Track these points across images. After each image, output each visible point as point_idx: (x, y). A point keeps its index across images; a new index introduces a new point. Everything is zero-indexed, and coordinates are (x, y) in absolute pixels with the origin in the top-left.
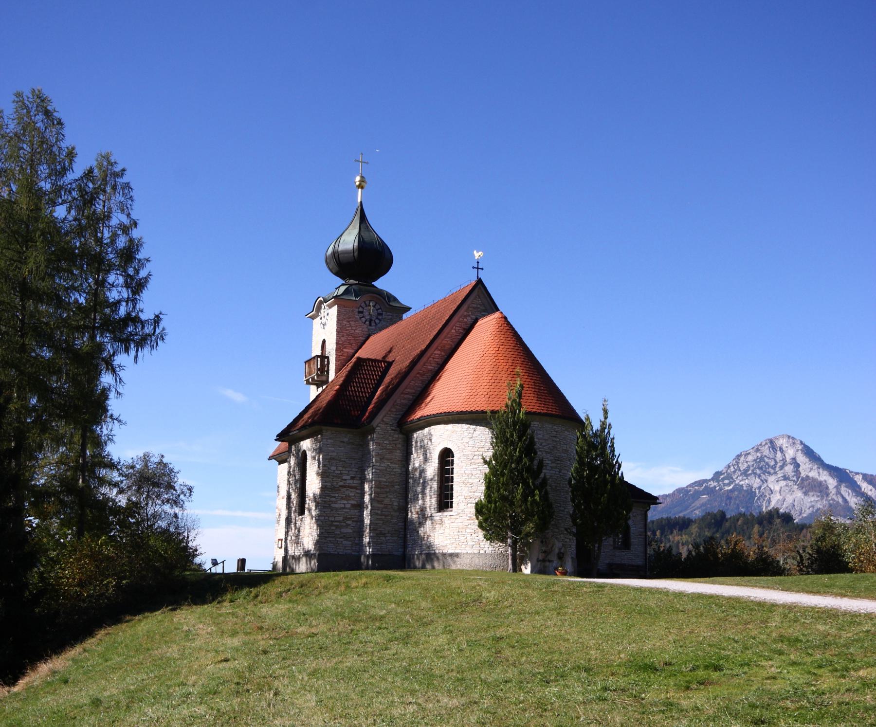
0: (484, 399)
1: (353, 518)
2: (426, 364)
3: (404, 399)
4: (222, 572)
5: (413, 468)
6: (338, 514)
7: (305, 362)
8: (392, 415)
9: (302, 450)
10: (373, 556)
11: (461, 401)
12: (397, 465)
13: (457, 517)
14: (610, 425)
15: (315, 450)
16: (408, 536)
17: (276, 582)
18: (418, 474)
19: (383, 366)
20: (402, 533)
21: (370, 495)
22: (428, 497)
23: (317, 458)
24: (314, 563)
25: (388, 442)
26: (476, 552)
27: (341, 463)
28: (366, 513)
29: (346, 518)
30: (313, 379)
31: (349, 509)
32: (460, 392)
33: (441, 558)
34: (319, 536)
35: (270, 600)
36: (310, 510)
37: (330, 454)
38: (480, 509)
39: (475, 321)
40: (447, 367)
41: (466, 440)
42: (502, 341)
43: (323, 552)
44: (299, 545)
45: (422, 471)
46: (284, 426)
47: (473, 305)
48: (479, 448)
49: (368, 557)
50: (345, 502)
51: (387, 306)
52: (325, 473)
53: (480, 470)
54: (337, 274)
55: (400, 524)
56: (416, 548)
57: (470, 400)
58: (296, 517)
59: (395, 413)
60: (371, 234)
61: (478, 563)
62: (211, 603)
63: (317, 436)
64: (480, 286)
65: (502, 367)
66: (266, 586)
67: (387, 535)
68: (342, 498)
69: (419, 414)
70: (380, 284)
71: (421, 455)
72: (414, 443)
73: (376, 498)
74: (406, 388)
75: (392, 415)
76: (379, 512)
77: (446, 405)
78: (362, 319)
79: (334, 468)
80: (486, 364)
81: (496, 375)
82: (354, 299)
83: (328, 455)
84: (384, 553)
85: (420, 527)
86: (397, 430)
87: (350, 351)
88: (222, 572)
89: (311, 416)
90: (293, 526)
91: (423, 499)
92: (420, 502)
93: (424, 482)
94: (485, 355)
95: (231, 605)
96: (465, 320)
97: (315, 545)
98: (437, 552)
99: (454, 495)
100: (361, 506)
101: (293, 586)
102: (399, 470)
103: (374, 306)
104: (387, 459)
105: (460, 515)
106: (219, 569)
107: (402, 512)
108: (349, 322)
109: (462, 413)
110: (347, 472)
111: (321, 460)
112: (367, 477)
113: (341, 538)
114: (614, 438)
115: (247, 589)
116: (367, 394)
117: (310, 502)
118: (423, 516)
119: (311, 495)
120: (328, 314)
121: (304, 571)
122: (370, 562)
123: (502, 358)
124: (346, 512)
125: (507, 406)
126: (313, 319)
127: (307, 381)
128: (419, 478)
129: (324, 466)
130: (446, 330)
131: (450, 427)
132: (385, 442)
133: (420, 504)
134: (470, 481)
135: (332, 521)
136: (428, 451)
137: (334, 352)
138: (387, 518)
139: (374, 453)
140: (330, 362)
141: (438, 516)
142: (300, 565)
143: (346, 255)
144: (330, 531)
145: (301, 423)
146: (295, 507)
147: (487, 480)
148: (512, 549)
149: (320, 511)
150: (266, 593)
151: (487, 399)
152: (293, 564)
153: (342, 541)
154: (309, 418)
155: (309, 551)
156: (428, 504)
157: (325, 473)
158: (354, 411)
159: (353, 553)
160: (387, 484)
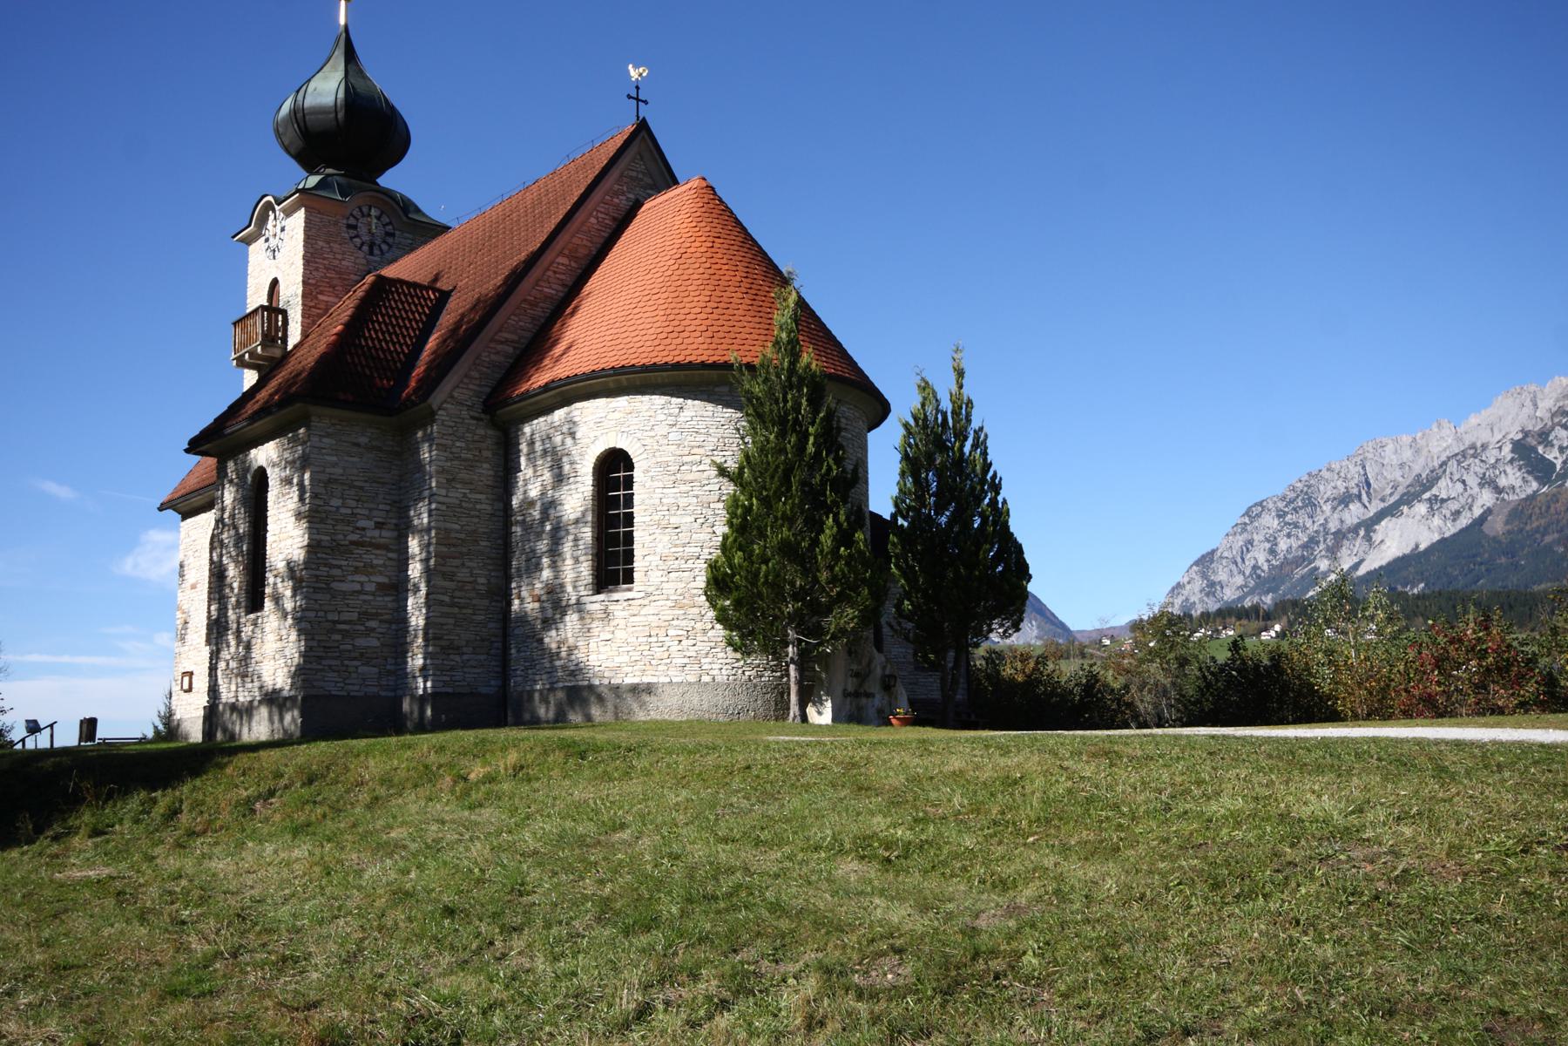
0: (701, 340)
1: (381, 615)
3: (495, 354)
4: (48, 746)
6: (348, 605)
7: (235, 324)
8: (471, 386)
9: (255, 466)
10: (434, 697)
11: (649, 343)
13: (646, 602)
14: (970, 402)
16: (513, 651)
17: (229, 771)
19: (432, 297)
21: (426, 561)
22: (569, 562)
23: (295, 481)
24: (292, 719)
25: (463, 445)
26: (692, 679)
27: (353, 492)
29: (365, 616)
30: (252, 354)
31: (373, 594)
35: (218, 823)
36: (277, 599)
37: (328, 470)
38: (719, 583)
39: (636, 207)
40: (587, 288)
44: (249, 680)
45: (550, 506)
46: (207, 420)
48: (693, 447)
49: (422, 700)
50: (363, 578)
51: (404, 219)
52: (317, 511)
53: (697, 497)
55: (491, 625)
56: (538, 677)
58: (239, 617)
59: (477, 382)
61: (700, 705)
62: (31, 842)
66: (198, 782)
67: (465, 650)
68: (357, 570)
69: (540, 379)
70: (390, 180)
72: (524, 447)
73: (439, 568)
74: (500, 331)
75: (471, 386)
76: (446, 599)
77: (611, 354)
83: (323, 472)
86: (481, 420)
88: (48, 746)
90: (231, 638)
91: (554, 566)
92: (546, 574)
95: (96, 846)
96: (616, 200)
97: (293, 678)
100: (399, 588)
101: (283, 782)
103: (378, 218)
104: (464, 482)
105: (652, 598)
106: (42, 741)
108: (329, 243)
110: (367, 512)
111: (307, 482)
112: (416, 522)
113: (355, 659)
114: (981, 429)
115: (143, 794)
116: (405, 348)
117: (279, 580)
118: (555, 605)
119: (281, 566)
120: (283, 229)
121: (263, 738)
122: (429, 712)
124: (365, 601)
126: (249, 244)
128: (542, 522)
129: (314, 496)
130: (580, 216)
131: (622, 402)
132: (458, 444)
134: (674, 520)
136: (565, 459)
137: (299, 299)
138: (464, 611)
139: (433, 468)
140: (290, 321)
141: (595, 603)
142: (254, 724)
143: (320, 116)
145: (251, 408)
146: (238, 595)
149: (305, 598)
150: (203, 803)
151: (709, 341)
153: (357, 667)
155: (276, 692)
156: (568, 573)
157: (317, 511)
158: (381, 379)
159: (383, 694)
160: (463, 536)
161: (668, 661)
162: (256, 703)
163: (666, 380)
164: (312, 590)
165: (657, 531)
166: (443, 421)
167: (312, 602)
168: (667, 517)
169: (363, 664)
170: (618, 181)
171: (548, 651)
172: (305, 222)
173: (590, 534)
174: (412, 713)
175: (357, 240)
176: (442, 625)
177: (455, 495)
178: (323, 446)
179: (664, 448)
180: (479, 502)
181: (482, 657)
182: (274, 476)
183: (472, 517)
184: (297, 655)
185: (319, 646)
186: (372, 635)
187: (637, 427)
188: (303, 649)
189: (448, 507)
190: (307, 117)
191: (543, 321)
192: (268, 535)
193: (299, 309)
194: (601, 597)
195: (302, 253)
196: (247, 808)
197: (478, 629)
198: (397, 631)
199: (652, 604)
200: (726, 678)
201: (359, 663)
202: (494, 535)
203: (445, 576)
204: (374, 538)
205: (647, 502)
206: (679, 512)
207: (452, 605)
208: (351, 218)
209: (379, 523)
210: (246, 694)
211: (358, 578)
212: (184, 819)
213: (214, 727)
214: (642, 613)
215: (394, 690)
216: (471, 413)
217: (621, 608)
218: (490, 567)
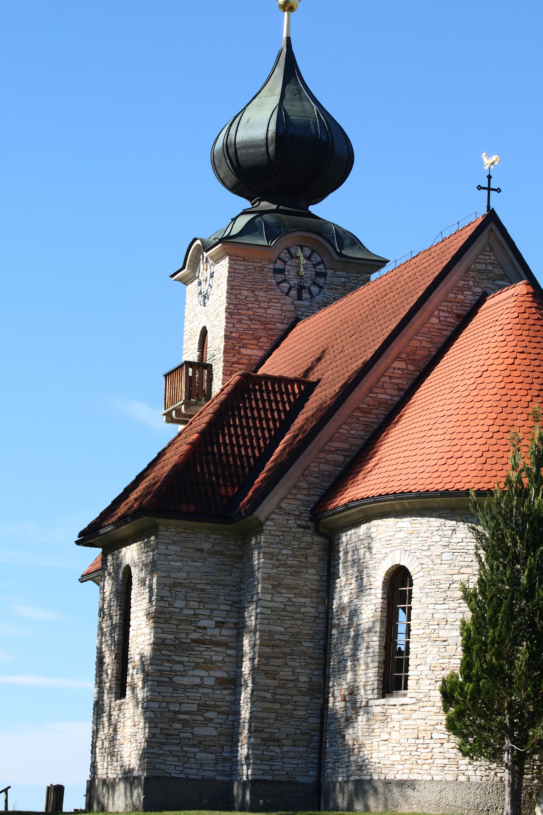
0: (473, 466)
2: (374, 390)
3: (324, 463)
5: (340, 605)
7: (166, 376)
8: (299, 496)
12: (307, 600)
13: (416, 707)
15: (145, 565)
16: (328, 745)
18: (346, 619)
19: (297, 391)
20: (316, 738)
21: (252, 659)
23: (147, 583)
24: (138, 793)
25: (290, 552)
26: (450, 778)
28: (245, 695)
29: (204, 707)
31: (212, 687)
32: (428, 451)
33: (380, 790)
34: (148, 741)
36: (133, 689)
41: (437, 550)
42: (524, 344)
43: (155, 773)
44: (115, 759)
45: (355, 613)
47: (479, 267)
49: (244, 785)
50: (203, 673)
51: (336, 257)
54: (236, 189)
56: (340, 770)
57: (444, 468)
58: (111, 702)
59: (306, 492)
60: (306, 104)
63: (150, 537)
64: (492, 225)
65: (517, 398)
67: (284, 742)
68: (197, 666)
71: (353, 581)
72: (341, 554)
74: (330, 440)
76: (269, 695)
78: (282, 285)
79: (182, 604)
80: (485, 391)
81: (504, 416)
82: (265, 243)
83: (169, 576)
84: (276, 779)
85: (347, 727)
86: (309, 528)
87: (255, 352)
89: (141, 496)
90: (105, 719)
91: (354, 669)
92: (349, 676)
93: (357, 635)
94: (485, 374)
98: (375, 777)
99: (410, 662)
102: (312, 610)
103: (308, 258)
104: (289, 587)
105: (421, 704)
107: (317, 695)
109: (427, 494)
110: (208, 612)
111: (154, 586)
112: (249, 623)
113: (194, 746)
116: (256, 451)
117: (135, 671)
119: (137, 658)
122: (248, 797)
123: (520, 379)
124: (204, 694)
125: (509, 482)
126: (186, 283)
127: (168, 415)
129: (160, 599)
131: (406, 522)
132: (284, 552)
133: (348, 680)
134: (443, 634)
135: (175, 712)
136: (365, 572)
138: (285, 707)
142: (116, 798)
144: (169, 732)
145: (122, 509)
147: (465, 634)
148: (512, 773)
151: (480, 467)
152: (104, 797)
153: (195, 753)
154: (136, 500)
155: (131, 771)
156: (361, 679)
157: (162, 613)
158: (226, 486)
159: (219, 778)
160: (286, 637)
161: (431, 761)
162: (117, 780)
163: (441, 505)
164: (156, 683)
165: (428, 643)
166: (271, 531)
167: (156, 694)
168: (437, 631)
169: (201, 751)
170: (465, 277)
171: (347, 748)
172: (229, 272)
173: (377, 643)
174: (238, 796)
176: (263, 718)
177: (280, 599)
178: (168, 552)
179: (437, 567)
181: (302, 749)
183: (297, 619)
184: (143, 740)
185: (161, 733)
186: (210, 724)
187: (416, 547)
188: (147, 735)
189: (272, 611)
190: (239, 152)
191: (376, 427)
192: (131, 629)
193: (221, 364)
194: (382, 701)
195: (225, 305)
197: (299, 723)
198: (233, 721)
199: (421, 709)
200: (479, 778)
201: (197, 750)
202: (317, 636)
203: (267, 674)
204: (215, 636)
205: (421, 616)
206: (447, 627)
207: (273, 701)
208: (279, 262)
209: (219, 622)
210: (113, 771)
211: (198, 672)
213: (92, 799)
214: (413, 717)
215: (230, 776)
216: (298, 522)
217: (396, 711)
218: (313, 667)
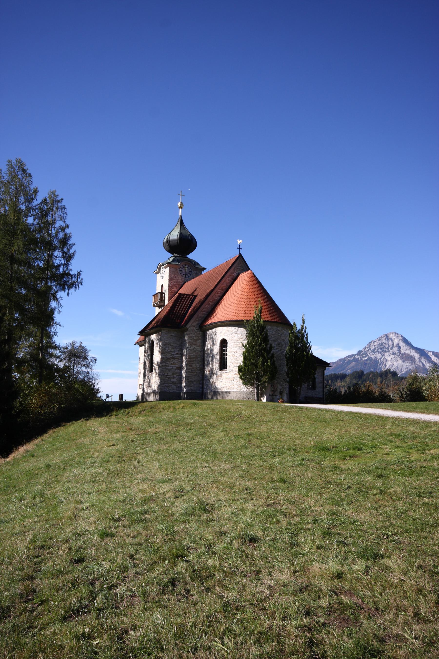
10: (187, 393)
21: (186, 362)
24: (158, 396)
26: (239, 391)
28: (184, 371)
29: (173, 374)
30: (157, 304)
34: (160, 383)
36: (155, 370)
38: (240, 369)
45: (212, 350)
49: (184, 393)
50: (173, 366)
64: (240, 257)
68: (172, 364)
69: (210, 322)
70: (191, 256)
85: (210, 378)
90: (147, 378)
91: (212, 364)
92: (211, 366)
93: (213, 356)
100: (181, 368)
103: (187, 268)
104: (194, 344)
106: (109, 400)
109: (231, 321)
118: (212, 373)
119: (156, 362)
125: (254, 318)
129: (162, 348)
130: (224, 280)
131: (225, 328)
134: (236, 355)
141: (219, 373)
145: (151, 326)
154: (155, 324)
155: (155, 390)
156: (214, 367)
170: (234, 270)
175: (182, 274)
180: (198, 349)
182: (155, 342)
194: (220, 372)
196: (140, 412)
211: (172, 366)
212: (130, 414)
